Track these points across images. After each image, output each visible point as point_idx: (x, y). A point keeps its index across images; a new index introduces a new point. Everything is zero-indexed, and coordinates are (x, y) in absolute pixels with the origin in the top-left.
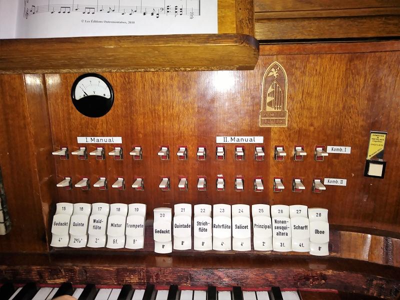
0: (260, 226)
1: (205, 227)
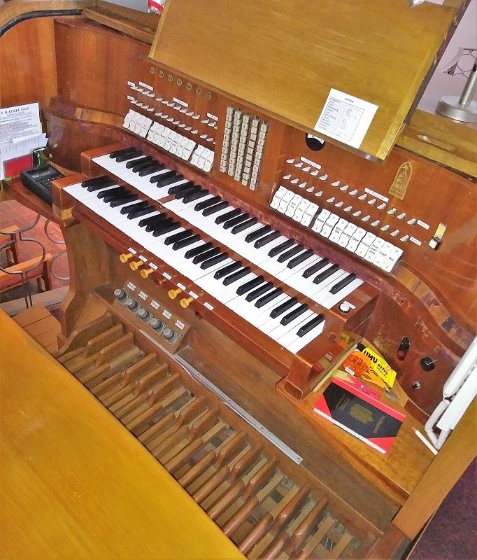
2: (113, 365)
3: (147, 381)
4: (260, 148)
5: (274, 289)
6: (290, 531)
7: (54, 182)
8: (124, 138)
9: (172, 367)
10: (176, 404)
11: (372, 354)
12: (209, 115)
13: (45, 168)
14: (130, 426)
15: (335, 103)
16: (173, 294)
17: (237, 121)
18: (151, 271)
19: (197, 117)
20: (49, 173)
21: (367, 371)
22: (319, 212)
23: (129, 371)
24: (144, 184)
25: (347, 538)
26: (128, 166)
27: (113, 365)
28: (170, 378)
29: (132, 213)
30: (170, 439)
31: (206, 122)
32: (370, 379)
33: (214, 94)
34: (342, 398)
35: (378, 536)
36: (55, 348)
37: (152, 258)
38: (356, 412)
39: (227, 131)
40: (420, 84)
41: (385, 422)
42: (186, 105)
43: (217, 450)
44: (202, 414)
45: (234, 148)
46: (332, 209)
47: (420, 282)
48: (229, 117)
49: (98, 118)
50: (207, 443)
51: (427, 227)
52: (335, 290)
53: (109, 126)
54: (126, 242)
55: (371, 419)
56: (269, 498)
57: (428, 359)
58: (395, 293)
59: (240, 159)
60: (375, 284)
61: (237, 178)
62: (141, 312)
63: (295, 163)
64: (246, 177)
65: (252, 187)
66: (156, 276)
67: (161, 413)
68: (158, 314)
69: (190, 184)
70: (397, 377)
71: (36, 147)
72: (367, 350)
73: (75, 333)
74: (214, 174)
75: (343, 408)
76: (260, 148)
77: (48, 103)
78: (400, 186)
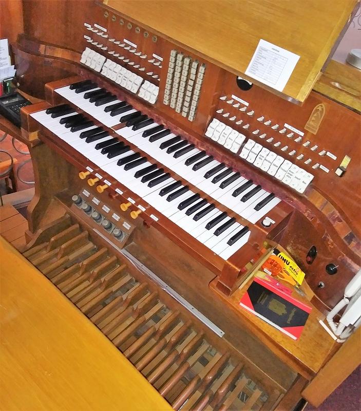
0: (282, 169)
1: (262, 158)
2: (72, 257)
4: (198, 86)
5: (201, 200)
6: (214, 389)
7: (22, 109)
8: (82, 72)
9: (121, 260)
10: (124, 288)
11: (286, 258)
12: (154, 55)
13: (14, 96)
14: (84, 310)
15: (264, 52)
16: (124, 207)
17: (179, 63)
18: (105, 187)
19: (144, 57)
20: (17, 100)
21: (281, 272)
22: (245, 141)
23: (85, 262)
24: (98, 113)
25: (257, 393)
26: (86, 97)
27: (72, 257)
28: (118, 269)
30: (119, 318)
31: (152, 61)
32: (284, 278)
33: (160, 39)
34: (262, 295)
35: (282, 392)
36: (22, 242)
37: (106, 176)
38: (274, 306)
39: (171, 70)
40: (336, 39)
41: (296, 313)
42: (135, 46)
43: (157, 326)
44: (144, 297)
45: (176, 85)
46: (257, 140)
47: (327, 202)
48: (172, 59)
49: (59, 53)
50: (148, 320)
51: (334, 158)
52: (258, 207)
53: (68, 61)
55: (285, 312)
56: (198, 362)
57: (332, 265)
58: (306, 210)
59: (181, 95)
60: (289, 202)
61: (178, 110)
62: (95, 215)
63: (227, 100)
64: (186, 109)
65: (191, 118)
66: (110, 192)
67: (112, 296)
68: (108, 216)
69: (103, 90)
70: (305, 277)
72: (282, 254)
73: (40, 231)
74: (158, 105)
75: (263, 302)
76: (198, 86)
77: (15, 39)
78: (314, 124)
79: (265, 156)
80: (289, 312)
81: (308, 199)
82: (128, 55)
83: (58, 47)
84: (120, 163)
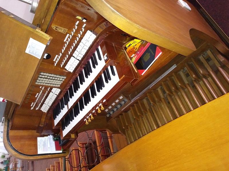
3: (139, 112)
11: (128, 45)
18: (102, 106)
21: (134, 48)
26: (75, 92)
29: (94, 94)
32: (137, 48)
37: (91, 111)
49: (43, 120)
51: (78, 22)
53: (46, 117)
54: (82, 122)
55: (149, 54)
66: (104, 105)
68: (117, 104)
69: (73, 83)
71: (52, 139)
75: (143, 64)
78: (62, 30)
79: (80, 50)
80: (150, 52)
81: (99, 34)
82: (74, 37)
83: (41, 119)
84: (107, 82)
